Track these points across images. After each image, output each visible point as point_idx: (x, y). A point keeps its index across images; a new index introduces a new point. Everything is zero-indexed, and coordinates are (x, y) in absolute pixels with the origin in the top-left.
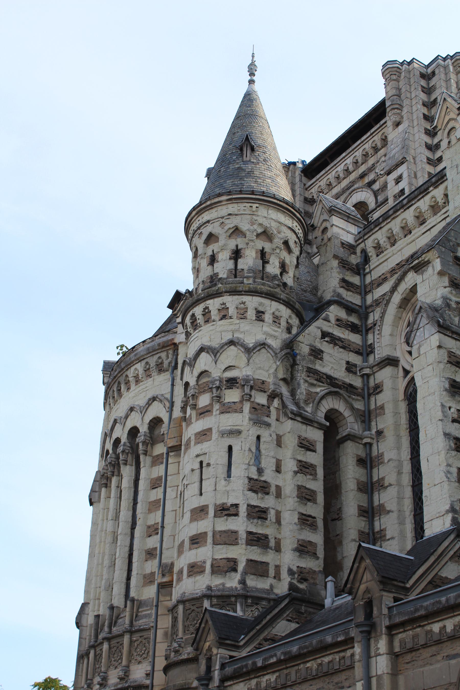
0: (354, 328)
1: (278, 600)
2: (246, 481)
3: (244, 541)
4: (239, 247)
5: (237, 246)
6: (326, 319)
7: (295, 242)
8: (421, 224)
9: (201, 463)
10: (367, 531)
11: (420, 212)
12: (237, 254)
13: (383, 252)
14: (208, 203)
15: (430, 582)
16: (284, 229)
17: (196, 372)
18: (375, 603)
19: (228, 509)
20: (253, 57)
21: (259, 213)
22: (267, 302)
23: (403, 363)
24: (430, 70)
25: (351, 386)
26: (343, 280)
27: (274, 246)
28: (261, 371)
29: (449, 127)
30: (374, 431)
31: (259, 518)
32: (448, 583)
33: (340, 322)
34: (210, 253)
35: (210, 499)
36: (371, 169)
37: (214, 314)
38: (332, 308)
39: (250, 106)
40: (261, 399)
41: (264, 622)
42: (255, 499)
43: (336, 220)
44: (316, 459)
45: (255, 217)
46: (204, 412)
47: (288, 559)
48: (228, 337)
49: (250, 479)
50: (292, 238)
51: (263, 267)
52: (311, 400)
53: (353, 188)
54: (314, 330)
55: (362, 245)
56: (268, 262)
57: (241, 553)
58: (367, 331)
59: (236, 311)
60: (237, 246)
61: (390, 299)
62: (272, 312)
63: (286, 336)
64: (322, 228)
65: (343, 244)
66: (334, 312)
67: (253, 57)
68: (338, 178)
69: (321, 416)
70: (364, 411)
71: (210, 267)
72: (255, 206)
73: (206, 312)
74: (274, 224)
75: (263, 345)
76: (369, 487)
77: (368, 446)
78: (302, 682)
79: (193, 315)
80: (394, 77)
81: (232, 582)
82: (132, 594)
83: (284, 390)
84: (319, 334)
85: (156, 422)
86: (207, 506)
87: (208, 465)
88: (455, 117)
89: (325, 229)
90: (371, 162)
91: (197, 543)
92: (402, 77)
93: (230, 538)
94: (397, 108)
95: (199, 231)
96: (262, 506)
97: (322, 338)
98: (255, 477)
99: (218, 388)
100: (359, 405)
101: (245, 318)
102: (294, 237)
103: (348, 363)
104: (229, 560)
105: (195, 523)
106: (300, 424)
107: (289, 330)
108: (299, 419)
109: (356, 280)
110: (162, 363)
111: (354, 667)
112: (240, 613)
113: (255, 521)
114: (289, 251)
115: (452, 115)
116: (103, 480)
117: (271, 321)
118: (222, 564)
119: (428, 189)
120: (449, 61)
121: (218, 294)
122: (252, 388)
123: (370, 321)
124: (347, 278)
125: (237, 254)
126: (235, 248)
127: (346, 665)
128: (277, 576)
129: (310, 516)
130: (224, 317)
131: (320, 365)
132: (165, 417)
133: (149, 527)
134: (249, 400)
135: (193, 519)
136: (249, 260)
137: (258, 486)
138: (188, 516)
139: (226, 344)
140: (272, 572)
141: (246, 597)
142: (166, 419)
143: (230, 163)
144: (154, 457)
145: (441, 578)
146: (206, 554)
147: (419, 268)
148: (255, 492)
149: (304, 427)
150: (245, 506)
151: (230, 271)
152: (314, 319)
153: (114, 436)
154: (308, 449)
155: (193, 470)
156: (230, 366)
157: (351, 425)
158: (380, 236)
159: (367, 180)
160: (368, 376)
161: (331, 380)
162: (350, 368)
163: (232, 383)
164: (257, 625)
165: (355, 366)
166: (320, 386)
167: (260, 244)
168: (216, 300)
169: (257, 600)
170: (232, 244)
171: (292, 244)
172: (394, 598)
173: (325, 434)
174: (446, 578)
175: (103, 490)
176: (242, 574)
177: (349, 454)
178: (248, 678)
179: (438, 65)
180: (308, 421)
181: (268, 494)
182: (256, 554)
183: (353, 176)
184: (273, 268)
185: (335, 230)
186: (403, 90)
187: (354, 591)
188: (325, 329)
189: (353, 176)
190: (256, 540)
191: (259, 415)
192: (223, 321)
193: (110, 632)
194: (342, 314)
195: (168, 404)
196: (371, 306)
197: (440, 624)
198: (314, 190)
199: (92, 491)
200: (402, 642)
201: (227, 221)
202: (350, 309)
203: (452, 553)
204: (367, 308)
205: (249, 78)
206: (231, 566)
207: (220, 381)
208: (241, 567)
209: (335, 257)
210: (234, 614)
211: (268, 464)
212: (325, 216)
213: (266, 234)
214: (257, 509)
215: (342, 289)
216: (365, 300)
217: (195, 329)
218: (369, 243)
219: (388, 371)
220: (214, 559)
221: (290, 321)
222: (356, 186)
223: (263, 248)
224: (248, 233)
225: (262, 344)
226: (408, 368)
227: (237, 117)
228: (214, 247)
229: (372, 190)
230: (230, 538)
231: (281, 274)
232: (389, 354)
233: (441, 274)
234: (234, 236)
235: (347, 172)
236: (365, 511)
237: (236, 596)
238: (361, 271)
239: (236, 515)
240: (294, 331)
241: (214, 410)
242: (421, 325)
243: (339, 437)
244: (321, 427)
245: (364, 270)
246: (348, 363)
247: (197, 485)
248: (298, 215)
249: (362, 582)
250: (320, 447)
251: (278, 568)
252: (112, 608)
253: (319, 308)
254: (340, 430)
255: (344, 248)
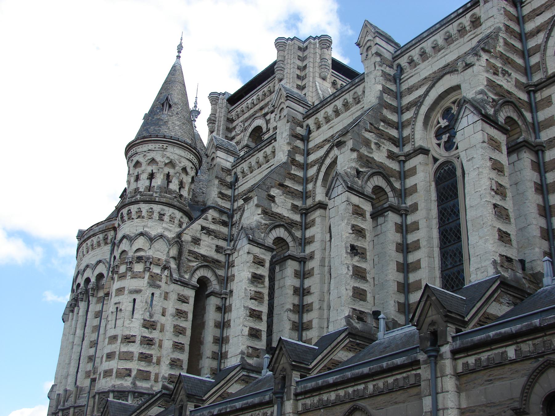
0: (224, 224)
1: (153, 395)
2: (142, 321)
3: (137, 359)
4: (154, 171)
5: (152, 170)
6: (206, 219)
7: (191, 167)
8: (267, 162)
9: (117, 308)
10: (217, 351)
11: (267, 155)
12: (152, 176)
13: (245, 176)
14: (137, 142)
15: (220, 396)
16: (183, 160)
17: (120, 251)
18: (184, 407)
19: (129, 338)
20: (181, 40)
21: (168, 150)
22: (166, 208)
23: (433, 152)
24: (305, 45)
25: (218, 261)
26: (220, 193)
27: (176, 172)
28: (158, 252)
29: (368, 45)
30: (229, 290)
31: (148, 344)
32: (493, 321)
33: (214, 221)
34: (136, 174)
35: (119, 332)
36: (266, 105)
37: (134, 215)
38: (210, 211)
39: (174, 75)
40: (156, 270)
41: (142, 408)
42: (146, 333)
43: (220, 154)
44: (189, 308)
45: (165, 153)
46: (122, 277)
47: (165, 370)
48: (140, 230)
49: (145, 320)
50: (189, 165)
51: (168, 185)
52: (189, 271)
53: (255, 116)
54: (196, 226)
55: (235, 170)
56: (171, 182)
57: (135, 366)
58: (232, 225)
59: (147, 213)
60: (152, 170)
61: (423, 101)
62: (169, 214)
63: (178, 230)
64: (211, 158)
65: (223, 169)
66: (211, 214)
67: (181, 40)
68: (243, 111)
69: (194, 281)
70: (224, 277)
71: (135, 183)
72: (165, 145)
73: (129, 212)
74: (176, 157)
75: (161, 236)
76: (223, 325)
77: (224, 299)
78: (409, 388)
79: (122, 213)
80: (281, 48)
81: (127, 383)
82: (78, 383)
83: (173, 265)
84: (200, 228)
85: (100, 276)
86: (117, 335)
87: (121, 310)
88: (372, 39)
89: (213, 159)
90: (267, 100)
91: (110, 358)
92: (287, 48)
93: (127, 356)
94: (281, 70)
95: (131, 159)
96: (151, 337)
97: (201, 231)
98: (148, 319)
99: (131, 262)
100: (298, 234)
101: (152, 218)
102: (191, 165)
103: (217, 246)
104: (126, 369)
105: (110, 345)
106: (180, 286)
107: (180, 226)
108: (179, 283)
109: (229, 192)
110: (107, 238)
111: (420, 385)
112: (130, 402)
113: (145, 346)
114: (187, 174)
115: (282, 100)
116: (72, 306)
117: (168, 221)
118: (122, 371)
119: (271, 141)
120: (317, 41)
121: (137, 202)
122: (151, 263)
123: (234, 219)
124: (223, 191)
125: (152, 176)
126: (151, 172)
127: (523, 356)
128: (156, 381)
129: (180, 343)
130: (139, 217)
131: (198, 248)
132: (105, 273)
133: (91, 342)
134: (149, 271)
135: (110, 343)
136: (158, 181)
137: (149, 325)
138: (107, 340)
139: (138, 235)
140: (153, 377)
141: (134, 393)
142: (105, 275)
143: (155, 115)
144: (98, 298)
145: (228, 393)
146: (114, 365)
147: (340, 144)
148: (147, 328)
149: (183, 288)
150: (140, 337)
151: (146, 187)
152: (198, 218)
153: (77, 283)
154: (184, 302)
155: (112, 312)
156: (139, 249)
157: (215, 286)
158: (245, 166)
159: (264, 112)
160: (229, 255)
161: (204, 258)
162: (219, 249)
163: (140, 259)
164: (138, 410)
165: (222, 248)
166: (196, 262)
167: (167, 170)
168: (135, 205)
169: (141, 394)
170: (149, 169)
171: (189, 170)
172: (456, 329)
173: (196, 292)
174: (231, 393)
175: (71, 314)
176: (133, 379)
177: (213, 302)
178: (489, 348)
179: (310, 43)
180: (185, 284)
181: (155, 329)
182: (143, 366)
183: (257, 107)
184: (174, 186)
185: (218, 159)
186: (287, 57)
187: (176, 399)
188: (205, 225)
189: (257, 107)
190: (145, 358)
191: (154, 281)
192: (139, 219)
193: (64, 405)
194: (216, 215)
195: (107, 266)
196: (236, 210)
197: (328, 395)
198: (234, 113)
199: (64, 314)
200: (466, 365)
201: (148, 154)
202: (221, 211)
203: (237, 378)
204: (234, 211)
205: (177, 54)
206: (128, 372)
207: (132, 258)
208: (134, 373)
209: (217, 177)
210: (127, 403)
211: (157, 309)
212: (214, 150)
213: (171, 164)
214: (147, 339)
215: (219, 199)
216: (233, 206)
217: (123, 223)
218: (239, 170)
219: (420, 158)
220: (118, 369)
221: (181, 220)
222: (257, 115)
223: (169, 173)
224: (159, 163)
225: (161, 235)
226: (437, 156)
227: (166, 82)
228: (139, 170)
229: (266, 119)
230: (127, 356)
231: (180, 189)
232: (422, 145)
233: (257, 206)
234: (151, 164)
235: (254, 105)
236: (219, 340)
237: (129, 392)
238: (398, 81)
239: (134, 342)
240: (184, 226)
241: (128, 275)
242: (336, 185)
243: (207, 293)
244: (193, 287)
245: (235, 186)
246: (217, 246)
247: (114, 322)
248: (194, 151)
249: (428, 315)
250: (192, 301)
251: (157, 375)
252: (66, 391)
253: (205, 210)
254: (208, 288)
255: (223, 171)
